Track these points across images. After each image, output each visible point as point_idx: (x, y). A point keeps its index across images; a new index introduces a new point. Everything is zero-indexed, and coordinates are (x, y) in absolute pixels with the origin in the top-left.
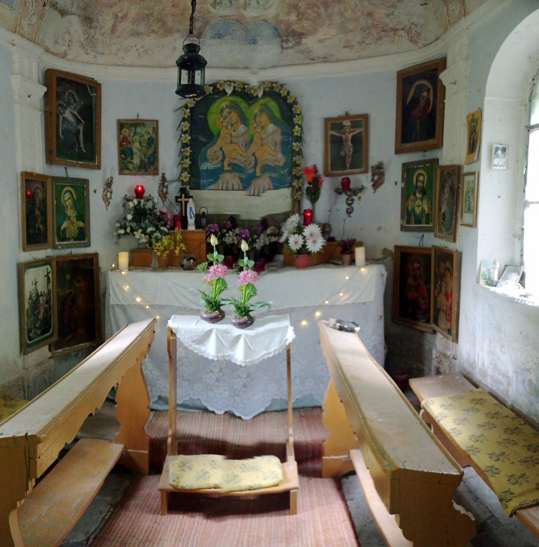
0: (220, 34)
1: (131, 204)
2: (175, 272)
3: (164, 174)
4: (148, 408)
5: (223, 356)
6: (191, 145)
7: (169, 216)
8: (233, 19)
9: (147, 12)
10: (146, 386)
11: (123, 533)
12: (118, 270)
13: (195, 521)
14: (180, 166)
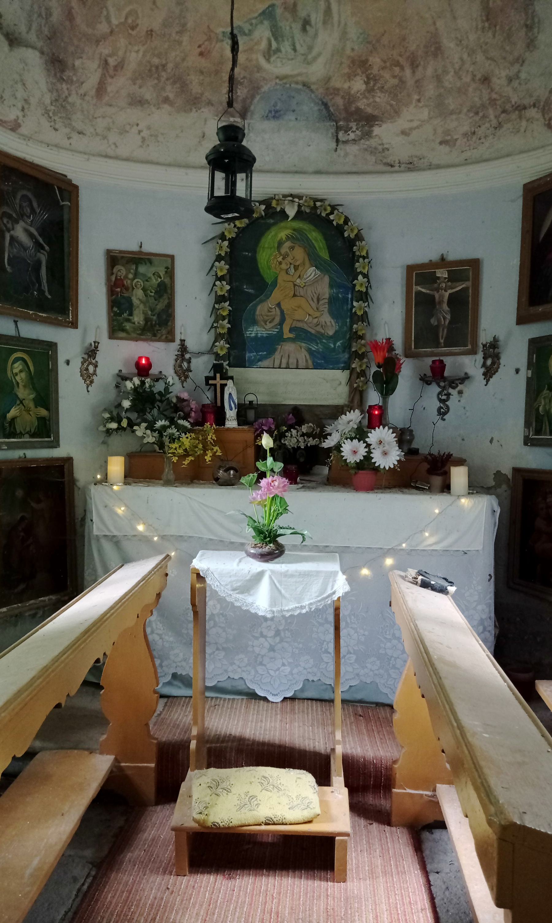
0: (276, 112)
1: (129, 385)
2: (205, 488)
3: (184, 340)
4: (155, 692)
5: (282, 611)
6: (230, 299)
7: (193, 405)
8: (297, 83)
9: (156, 61)
10: (152, 658)
11: (112, 915)
12: (107, 484)
13: (234, 886)
14: (213, 330)
